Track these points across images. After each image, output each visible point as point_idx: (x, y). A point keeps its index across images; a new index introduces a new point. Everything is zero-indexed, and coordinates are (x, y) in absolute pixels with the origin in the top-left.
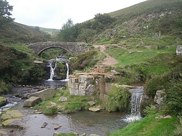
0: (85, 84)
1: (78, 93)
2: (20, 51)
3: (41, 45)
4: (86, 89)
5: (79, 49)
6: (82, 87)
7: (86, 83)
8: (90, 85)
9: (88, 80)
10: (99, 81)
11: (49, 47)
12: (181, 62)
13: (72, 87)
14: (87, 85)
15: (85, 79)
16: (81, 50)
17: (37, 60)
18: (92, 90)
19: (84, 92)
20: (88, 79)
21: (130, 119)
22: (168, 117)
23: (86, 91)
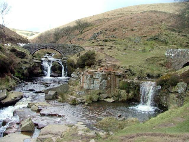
0: (100, 80)
1: (93, 87)
2: (21, 51)
3: (35, 46)
4: (101, 84)
5: (70, 50)
6: (97, 82)
7: (100, 78)
8: (104, 81)
9: (102, 76)
10: (111, 77)
11: (43, 48)
12: (188, 2)
13: (88, 82)
14: (102, 81)
15: (100, 75)
16: (71, 51)
17: (35, 59)
18: (106, 84)
19: (99, 86)
20: (102, 75)
21: (141, 108)
22: (172, 133)
23: (101, 85)
